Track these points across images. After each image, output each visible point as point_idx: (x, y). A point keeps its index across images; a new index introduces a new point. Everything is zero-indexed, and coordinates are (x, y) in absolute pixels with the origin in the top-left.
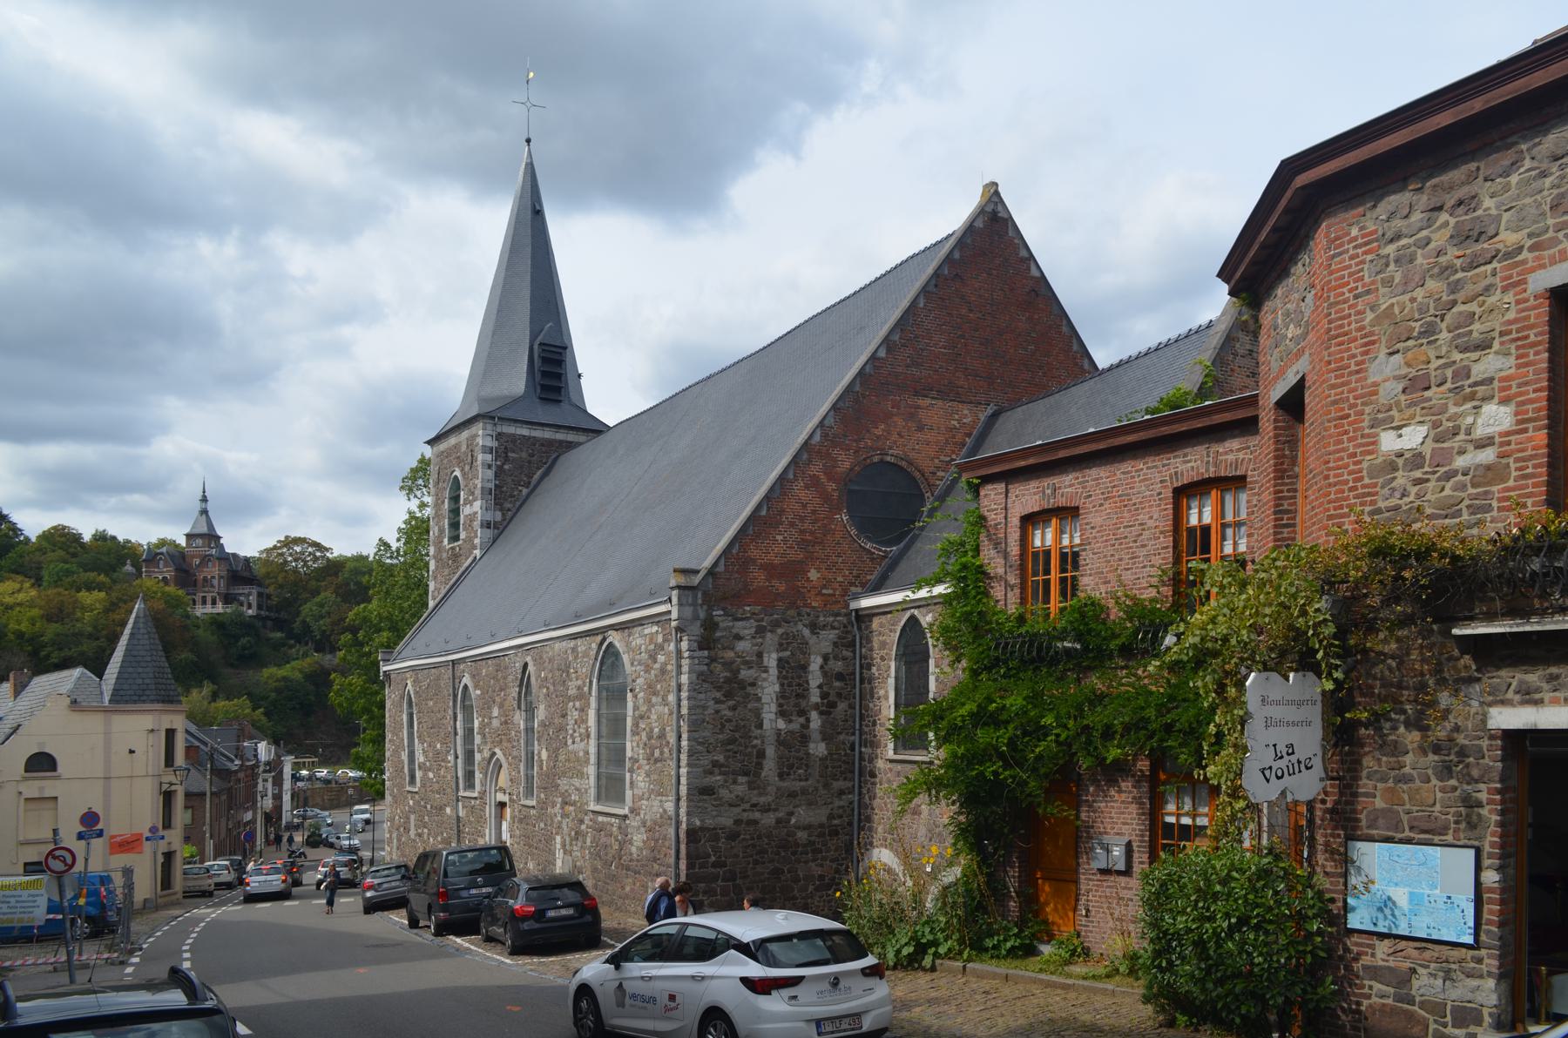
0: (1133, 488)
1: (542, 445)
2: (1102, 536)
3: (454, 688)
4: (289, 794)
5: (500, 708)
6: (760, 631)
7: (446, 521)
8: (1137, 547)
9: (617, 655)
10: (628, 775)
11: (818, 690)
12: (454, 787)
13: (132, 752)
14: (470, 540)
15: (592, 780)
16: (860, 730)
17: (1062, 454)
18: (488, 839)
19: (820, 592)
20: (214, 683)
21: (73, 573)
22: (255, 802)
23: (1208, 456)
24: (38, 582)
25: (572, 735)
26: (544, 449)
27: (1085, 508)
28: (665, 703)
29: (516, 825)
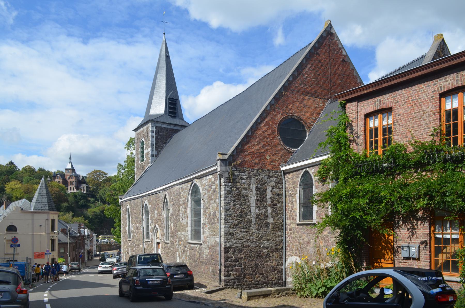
0: (419, 96)
1: (170, 130)
2: (404, 118)
3: (142, 205)
4: (95, 246)
5: (157, 211)
6: (250, 177)
7: (140, 155)
8: (421, 121)
9: (197, 188)
10: (202, 230)
11: (270, 199)
12: (143, 238)
13: (41, 226)
14: (147, 161)
15: (189, 232)
16: (285, 214)
17: (385, 85)
18: (154, 252)
19: (270, 164)
20: (73, 212)
21: (32, 179)
22: (84, 247)
23: (457, 77)
24: (22, 182)
25: (182, 217)
26: (170, 132)
27: (395, 107)
28: (215, 202)
29: (163, 250)
